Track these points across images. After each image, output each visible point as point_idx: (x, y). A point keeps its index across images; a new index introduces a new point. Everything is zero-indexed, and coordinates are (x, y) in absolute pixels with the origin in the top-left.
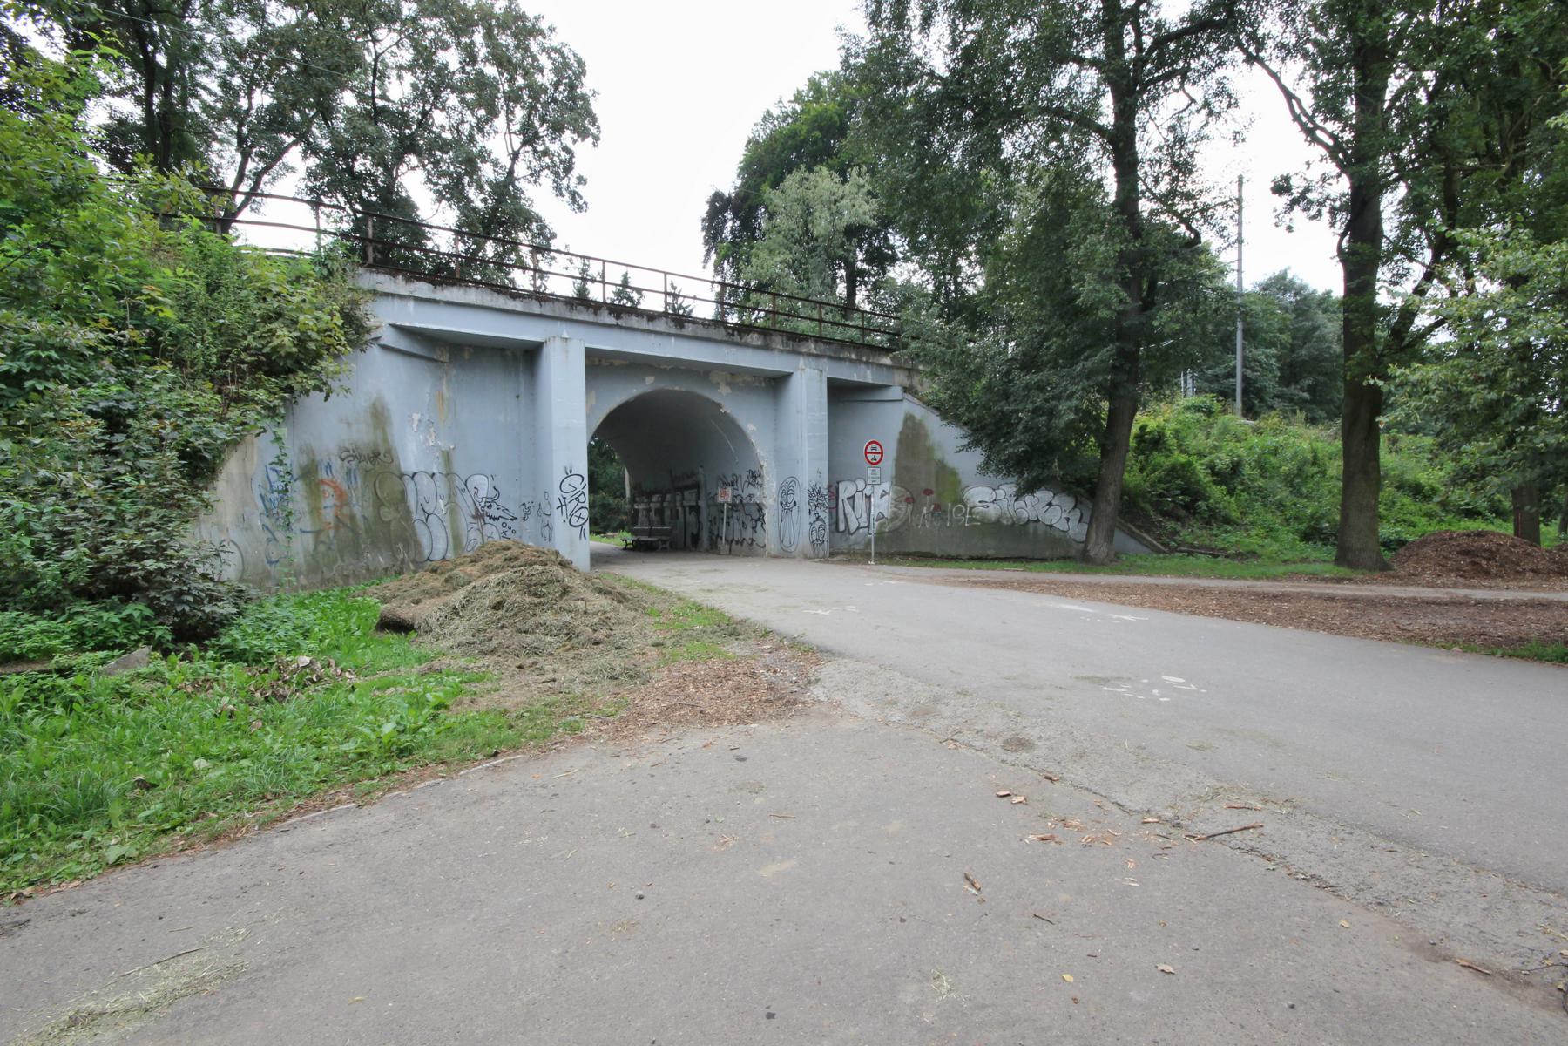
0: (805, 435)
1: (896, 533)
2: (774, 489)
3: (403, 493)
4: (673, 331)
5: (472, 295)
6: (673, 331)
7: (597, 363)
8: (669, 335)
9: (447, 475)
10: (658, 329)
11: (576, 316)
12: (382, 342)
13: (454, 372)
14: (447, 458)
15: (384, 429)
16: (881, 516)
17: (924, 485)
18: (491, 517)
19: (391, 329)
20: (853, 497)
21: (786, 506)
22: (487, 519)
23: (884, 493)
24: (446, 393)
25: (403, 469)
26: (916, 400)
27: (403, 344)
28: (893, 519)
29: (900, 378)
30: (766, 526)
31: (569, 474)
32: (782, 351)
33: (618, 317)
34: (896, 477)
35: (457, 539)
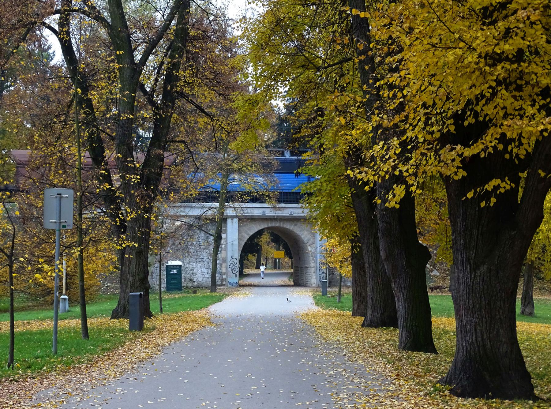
31: (232, 258)
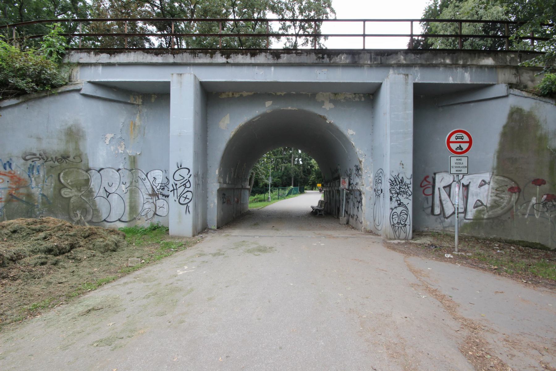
0: (388, 132)
1: (496, 221)
2: (371, 179)
3: (87, 181)
4: (271, 61)
5: (132, 57)
6: (271, 61)
7: (231, 95)
8: (269, 65)
9: (131, 170)
10: (258, 62)
11: (198, 60)
12: (82, 92)
13: (146, 110)
14: (133, 160)
15: (77, 143)
16: (479, 204)
17: (533, 175)
18: (163, 195)
19: (89, 85)
20: (450, 186)
21: (378, 192)
22: (160, 196)
23: (484, 183)
24: (137, 121)
25: (91, 165)
26: (524, 93)
27: (99, 93)
28: (492, 207)
29: (506, 76)
30: (363, 207)
31: (180, 167)
32: (371, 66)
33: (228, 57)
34: (498, 168)
35: (133, 209)
